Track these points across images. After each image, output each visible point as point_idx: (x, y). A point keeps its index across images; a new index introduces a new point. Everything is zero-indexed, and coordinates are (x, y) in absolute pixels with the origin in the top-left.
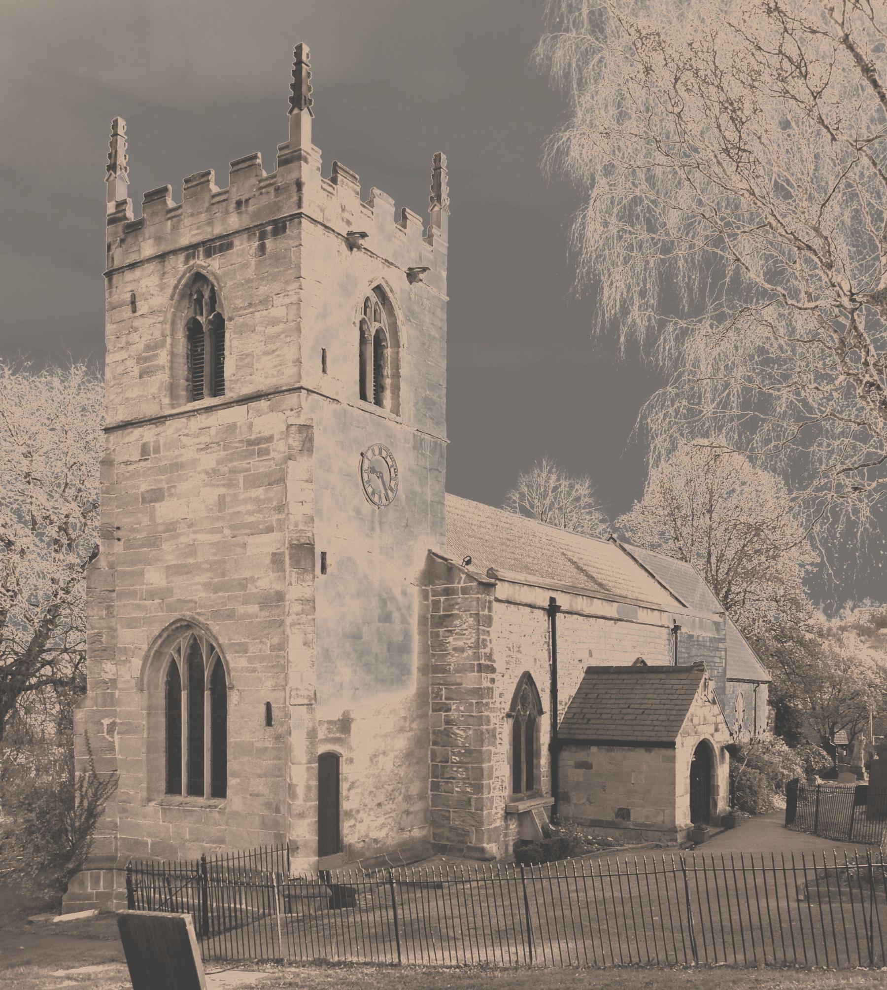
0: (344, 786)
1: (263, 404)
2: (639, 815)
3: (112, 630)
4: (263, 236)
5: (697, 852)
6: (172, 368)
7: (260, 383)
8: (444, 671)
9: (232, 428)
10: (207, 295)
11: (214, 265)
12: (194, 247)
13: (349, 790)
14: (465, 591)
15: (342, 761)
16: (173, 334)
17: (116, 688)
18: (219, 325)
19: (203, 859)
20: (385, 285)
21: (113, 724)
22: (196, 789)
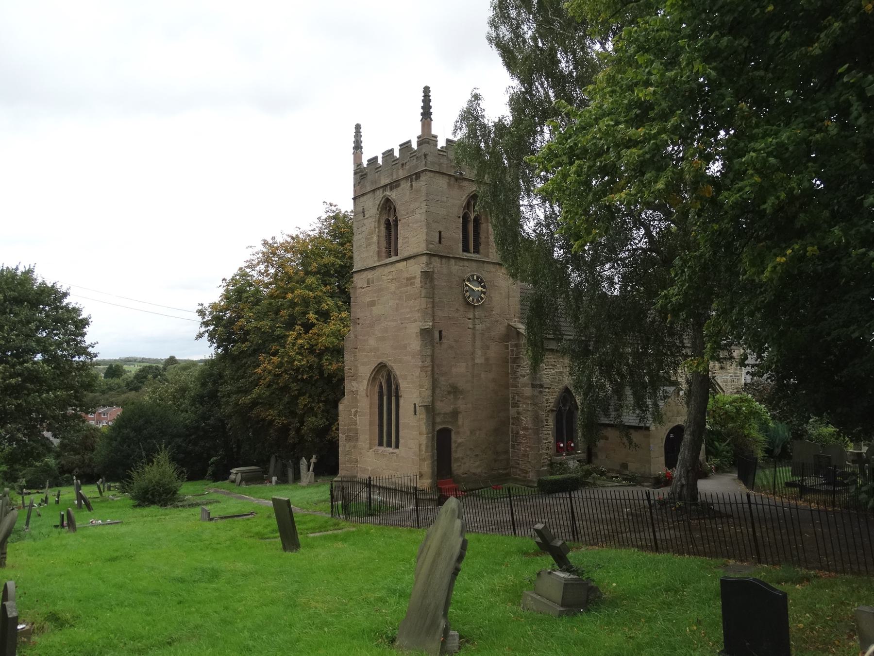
0: (453, 446)
1: (412, 261)
2: (633, 467)
3: (356, 367)
4: (411, 181)
5: (656, 491)
6: (378, 243)
7: (406, 254)
11: (393, 195)
12: (386, 186)
15: (453, 433)
16: (379, 227)
18: (396, 221)
19: (370, 478)
22: (389, 445)
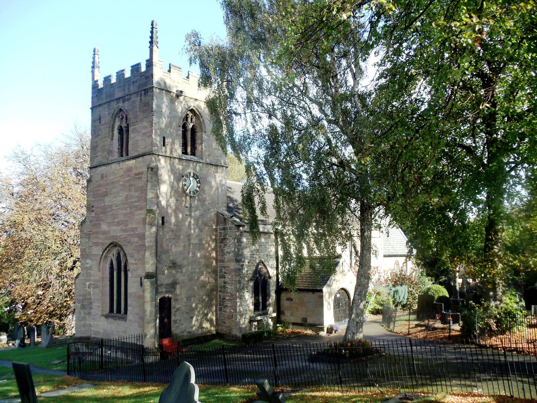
7: (141, 151)
8: (223, 261)
9: (129, 170)
10: (124, 116)
12: (119, 99)
13: (176, 312)
14: (230, 228)
17: (92, 270)
20: (194, 109)
21: (90, 284)
